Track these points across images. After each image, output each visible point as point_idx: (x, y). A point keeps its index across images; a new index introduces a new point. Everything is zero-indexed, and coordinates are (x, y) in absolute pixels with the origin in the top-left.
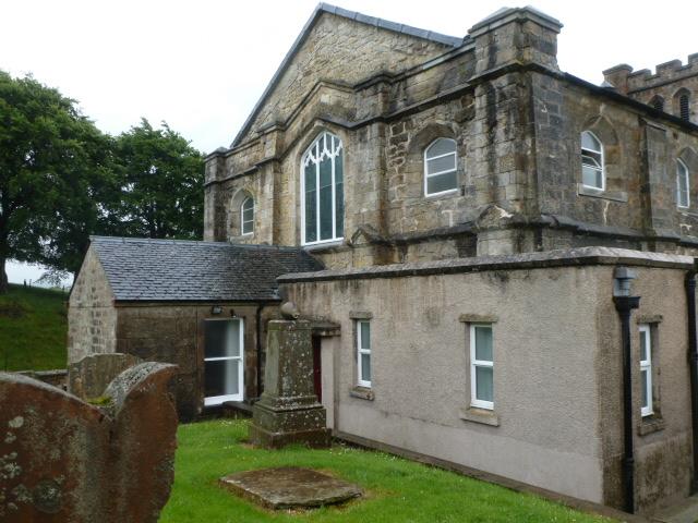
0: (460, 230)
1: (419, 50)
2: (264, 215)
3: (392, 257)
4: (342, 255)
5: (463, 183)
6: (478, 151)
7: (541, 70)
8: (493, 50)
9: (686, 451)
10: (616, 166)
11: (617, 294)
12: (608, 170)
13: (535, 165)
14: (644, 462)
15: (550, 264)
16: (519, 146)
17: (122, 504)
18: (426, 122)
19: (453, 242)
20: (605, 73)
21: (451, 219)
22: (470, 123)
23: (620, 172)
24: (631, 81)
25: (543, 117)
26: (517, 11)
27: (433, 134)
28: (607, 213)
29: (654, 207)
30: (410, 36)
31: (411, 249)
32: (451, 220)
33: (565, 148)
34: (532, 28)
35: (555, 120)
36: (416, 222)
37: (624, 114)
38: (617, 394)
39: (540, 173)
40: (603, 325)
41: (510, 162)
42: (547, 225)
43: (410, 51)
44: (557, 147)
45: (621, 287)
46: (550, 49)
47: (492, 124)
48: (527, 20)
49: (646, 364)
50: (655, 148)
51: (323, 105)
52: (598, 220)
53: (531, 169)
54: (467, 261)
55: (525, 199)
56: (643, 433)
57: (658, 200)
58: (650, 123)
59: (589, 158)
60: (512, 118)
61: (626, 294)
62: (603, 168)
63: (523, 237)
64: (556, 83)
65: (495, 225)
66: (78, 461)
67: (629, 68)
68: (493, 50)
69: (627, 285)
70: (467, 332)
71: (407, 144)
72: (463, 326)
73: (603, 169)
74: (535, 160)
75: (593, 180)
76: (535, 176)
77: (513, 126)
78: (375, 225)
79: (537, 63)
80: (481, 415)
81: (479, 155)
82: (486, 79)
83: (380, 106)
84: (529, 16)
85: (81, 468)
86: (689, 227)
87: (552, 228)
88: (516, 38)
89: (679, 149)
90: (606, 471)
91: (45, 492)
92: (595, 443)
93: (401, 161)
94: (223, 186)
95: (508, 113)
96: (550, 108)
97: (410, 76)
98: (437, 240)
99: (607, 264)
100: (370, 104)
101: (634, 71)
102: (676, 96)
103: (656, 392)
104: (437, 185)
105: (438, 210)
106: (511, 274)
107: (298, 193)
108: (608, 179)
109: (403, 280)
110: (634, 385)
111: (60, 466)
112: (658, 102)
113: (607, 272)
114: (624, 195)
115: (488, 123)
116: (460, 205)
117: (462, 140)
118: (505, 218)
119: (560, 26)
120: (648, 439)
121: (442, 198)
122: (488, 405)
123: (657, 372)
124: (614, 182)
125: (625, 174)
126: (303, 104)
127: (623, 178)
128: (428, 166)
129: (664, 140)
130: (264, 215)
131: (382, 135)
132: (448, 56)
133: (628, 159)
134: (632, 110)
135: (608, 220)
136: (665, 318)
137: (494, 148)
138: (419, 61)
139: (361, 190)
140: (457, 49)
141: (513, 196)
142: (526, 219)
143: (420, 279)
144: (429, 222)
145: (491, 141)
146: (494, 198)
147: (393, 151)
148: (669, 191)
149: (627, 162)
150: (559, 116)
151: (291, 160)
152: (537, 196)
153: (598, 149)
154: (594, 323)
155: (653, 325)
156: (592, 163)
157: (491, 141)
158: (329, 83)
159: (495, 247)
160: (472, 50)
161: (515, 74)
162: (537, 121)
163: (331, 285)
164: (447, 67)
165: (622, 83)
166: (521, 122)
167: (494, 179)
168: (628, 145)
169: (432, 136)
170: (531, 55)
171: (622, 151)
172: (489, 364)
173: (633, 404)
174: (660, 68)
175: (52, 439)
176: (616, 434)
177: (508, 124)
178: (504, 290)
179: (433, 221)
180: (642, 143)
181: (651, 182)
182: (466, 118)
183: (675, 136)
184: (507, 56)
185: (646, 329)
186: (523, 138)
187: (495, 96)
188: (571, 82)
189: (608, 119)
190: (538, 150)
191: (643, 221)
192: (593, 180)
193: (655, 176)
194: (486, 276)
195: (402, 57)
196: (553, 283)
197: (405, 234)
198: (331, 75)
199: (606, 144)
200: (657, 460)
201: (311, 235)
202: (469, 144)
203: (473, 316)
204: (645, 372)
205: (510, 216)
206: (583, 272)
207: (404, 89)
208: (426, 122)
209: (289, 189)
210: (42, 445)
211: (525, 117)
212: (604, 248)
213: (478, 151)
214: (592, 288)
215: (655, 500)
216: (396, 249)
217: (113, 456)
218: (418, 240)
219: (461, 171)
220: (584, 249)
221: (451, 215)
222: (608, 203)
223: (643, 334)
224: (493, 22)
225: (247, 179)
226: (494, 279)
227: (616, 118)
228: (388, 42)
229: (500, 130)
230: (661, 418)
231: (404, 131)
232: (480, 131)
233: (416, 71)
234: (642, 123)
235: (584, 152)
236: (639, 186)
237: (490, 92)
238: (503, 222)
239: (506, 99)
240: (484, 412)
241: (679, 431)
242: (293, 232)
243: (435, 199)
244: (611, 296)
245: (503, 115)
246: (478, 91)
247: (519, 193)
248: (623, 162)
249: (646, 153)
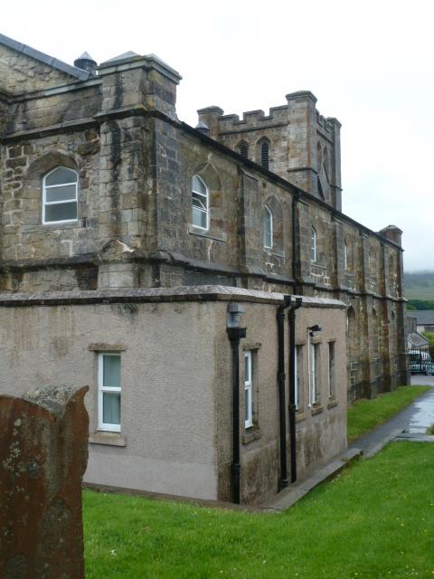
0: (79, 261)
1: (41, 74)
3: (6, 283)
5: (84, 215)
6: (101, 186)
7: (164, 118)
8: (119, 91)
9: (275, 456)
10: (219, 209)
11: (230, 326)
12: (212, 211)
13: (156, 206)
14: (246, 466)
15: (176, 299)
16: (141, 186)
17: (66, 471)
18: (47, 150)
19: (73, 272)
20: (200, 112)
21: (71, 249)
22: (93, 157)
23: (221, 215)
25: (163, 161)
26: (144, 59)
27: (54, 163)
28: (211, 251)
29: (247, 247)
30: (32, 59)
31: (26, 276)
32: (71, 249)
33: (180, 191)
34: (156, 77)
35: (173, 165)
36: (34, 250)
37: (227, 163)
38: (228, 410)
39: (159, 213)
40: (219, 352)
41: (133, 200)
42: (164, 261)
43: (31, 73)
44: (174, 190)
45: (233, 320)
46: (171, 98)
47: (116, 162)
48: (152, 68)
49: (248, 383)
50: (250, 196)
52: (203, 257)
53: (151, 208)
54: (89, 294)
55: (146, 236)
56: (246, 442)
57: (250, 238)
58: (246, 173)
59: (198, 201)
60: (136, 158)
61: (236, 325)
62: (208, 210)
63: (143, 271)
64: (175, 131)
65: (116, 258)
66: (46, 446)
67: (221, 111)
68: (119, 91)
69: (238, 318)
70: (96, 360)
71: (25, 169)
72: (92, 354)
73: (207, 210)
74: (155, 200)
75: (201, 220)
76: (155, 215)
77: (136, 166)
79: (160, 110)
80: (109, 438)
81: (103, 190)
82: (112, 118)
84: (154, 66)
85: (47, 450)
86: (272, 265)
87: (168, 264)
88: (142, 85)
89: (267, 197)
90: (220, 476)
91: (32, 465)
92: (211, 453)
93: (18, 185)
95: (132, 153)
96: (169, 153)
97: (31, 99)
98: (55, 269)
99: (224, 301)
101: (225, 114)
102: (258, 142)
103: (255, 407)
104: (55, 212)
105: (58, 239)
106: (140, 306)
108: (211, 220)
109: (29, 310)
110: (241, 403)
111: (38, 449)
112: (244, 147)
113: (222, 307)
114: (224, 236)
115: (112, 160)
116: (81, 236)
117: (85, 172)
118: (127, 253)
119: (180, 78)
120: (249, 447)
121: (62, 227)
122: (115, 427)
123: (256, 391)
124: (217, 223)
125: (225, 217)
127: (224, 220)
128: (45, 193)
129: (256, 189)
132: (73, 87)
133: (229, 204)
134: (234, 160)
135: (212, 257)
136: (263, 344)
137: (117, 185)
138: (40, 85)
140: (82, 82)
141: (134, 233)
142: (146, 254)
143: (48, 309)
144: (47, 251)
145: (115, 178)
146: (117, 232)
147: (9, 174)
148: (258, 234)
149: (228, 204)
150: (176, 161)
152: (156, 234)
153: (205, 193)
154: (212, 351)
155: (254, 351)
156: (199, 205)
157: (115, 178)
159: (116, 280)
160: (97, 86)
161: (141, 118)
162: (158, 165)
164: (71, 98)
165: (214, 125)
166: (143, 164)
167: (117, 215)
168: (228, 191)
169: (51, 165)
170: (155, 102)
171: (223, 196)
172: (117, 389)
173: (240, 418)
174: (246, 115)
175: (34, 433)
176: (227, 443)
177: (132, 164)
178: (133, 321)
179: (52, 249)
180: (239, 190)
181: (246, 225)
182: (90, 151)
183: (264, 185)
184: (133, 99)
185: (248, 355)
186: (145, 179)
187: (120, 136)
188: (184, 128)
189: (214, 167)
190: (158, 192)
191: (238, 258)
192: (201, 220)
193: (250, 220)
194: (117, 309)
195: (23, 78)
196: (179, 316)
197: (20, 261)
199: (211, 189)
200: (256, 463)
202: (91, 178)
203: (102, 345)
204: (247, 391)
205: (132, 251)
206: (204, 307)
207: (24, 112)
208: (46, 149)
210: (29, 437)
211: (148, 160)
212: (221, 287)
213: (101, 186)
214: (210, 320)
215: (254, 498)
216: (10, 275)
217: (61, 442)
218: (35, 268)
219: (83, 203)
220: (206, 287)
221: (71, 245)
222: (212, 242)
223: (247, 358)
224: (122, 64)
226: (124, 311)
227: (220, 166)
229: (124, 168)
230: (258, 428)
231: (23, 155)
232: (104, 166)
233: (37, 95)
234: (240, 172)
235: (194, 195)
236: (236, 228)
237: (116, 132)
238: (125, 256)
239: (131, 140)
240: (111, 435)
241: (270, 439)
243: (55, 228)
244: (225, 328)
245: (127, 155)
246: (103, 127)
247: (140, 230)
248: (224, 205)
249: (242, 199)
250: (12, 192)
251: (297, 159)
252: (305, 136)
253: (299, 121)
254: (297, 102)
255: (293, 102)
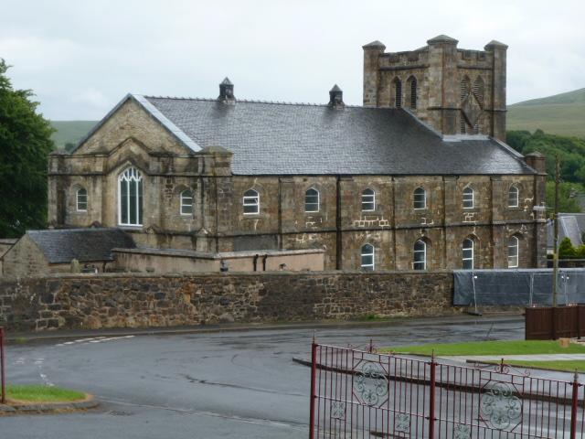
2: (96, 206)
4: (141, 235)
8: (204, 166)
20: (365, 48)
24: (381, 60)
31: (174, 237)
47: (203, 196)
51: (131, 152)
68: (204, 166)
78: (158, 225)
82: (201, 177)
83: (161, 168)
86: (312, 223)
94: (64, 178)
100: (155, 165)
101: (386, 51)
105: (185, 223)
107: (117, 195)
126: (120, 146)
130: (96, 206)
131: (161, 182)
139: (152, 207)
151: (112, 177)
157: (202, 202)
158: (135, 140)
163: (138, 256)
167: (203, 217)
198: (136, 135)
201: (124, 220)
209: (111, 192)
225: (82, 178)
228: (165, 134)
229: (205, 198)
233: (177, 156)
242: (114, 217)
250: (168, 199)
251: (434, 99)
252: (440, 79)
253: (436, 65)
254: (436, 48)
255: (432, 47)
